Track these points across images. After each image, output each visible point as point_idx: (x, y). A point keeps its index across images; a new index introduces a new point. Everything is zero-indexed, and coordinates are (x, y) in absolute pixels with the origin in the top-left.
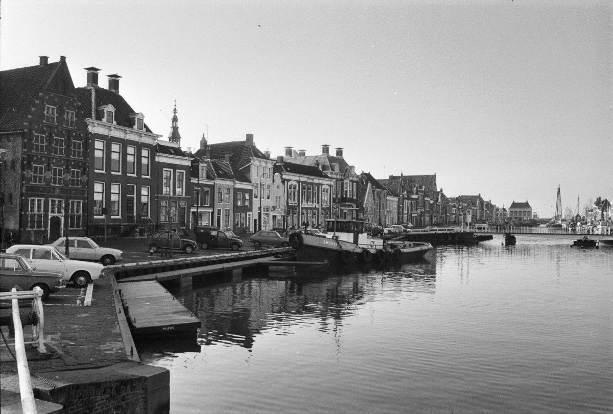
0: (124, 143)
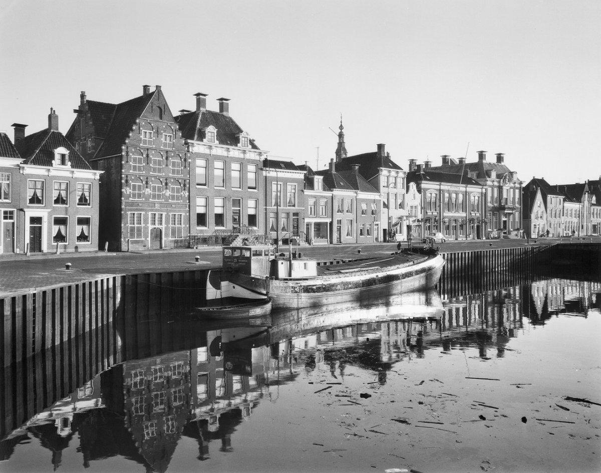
0: (226, 161)
